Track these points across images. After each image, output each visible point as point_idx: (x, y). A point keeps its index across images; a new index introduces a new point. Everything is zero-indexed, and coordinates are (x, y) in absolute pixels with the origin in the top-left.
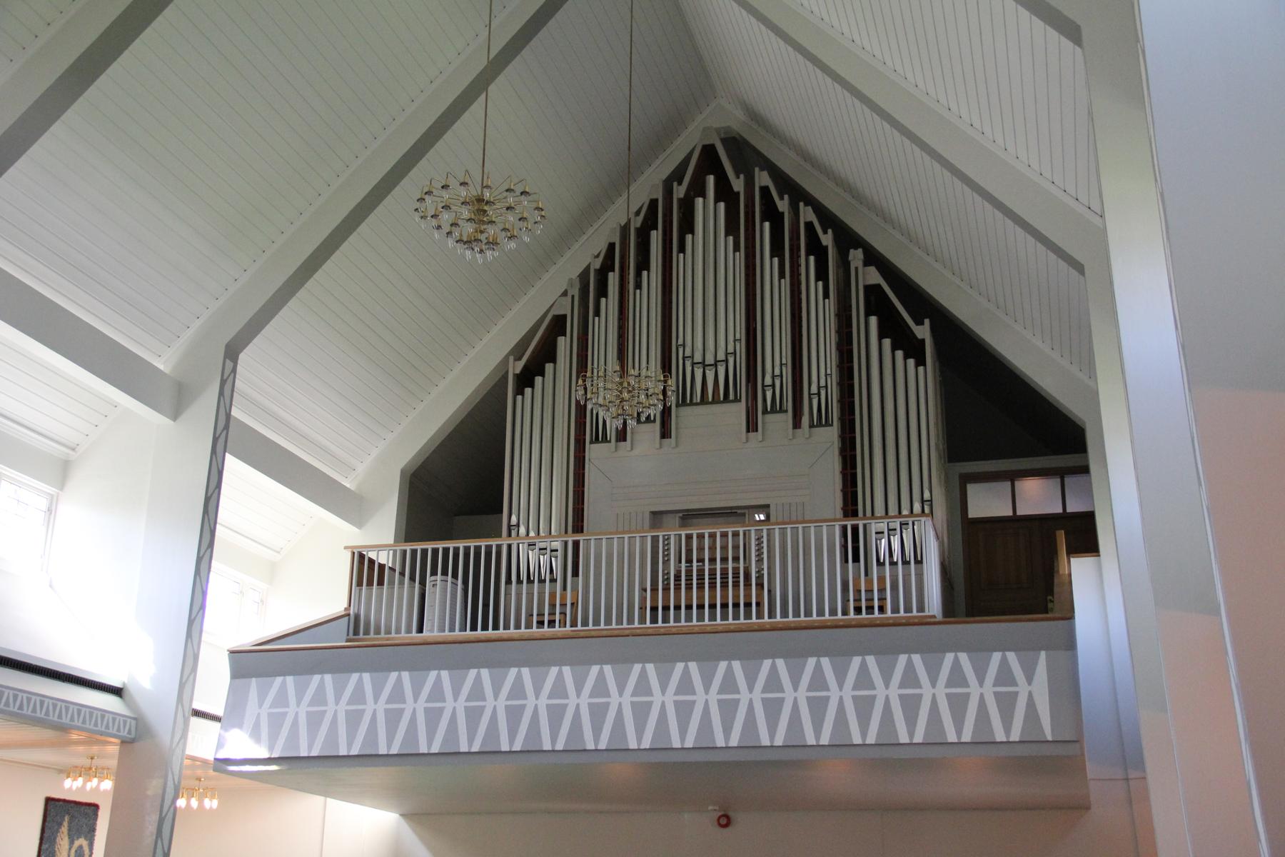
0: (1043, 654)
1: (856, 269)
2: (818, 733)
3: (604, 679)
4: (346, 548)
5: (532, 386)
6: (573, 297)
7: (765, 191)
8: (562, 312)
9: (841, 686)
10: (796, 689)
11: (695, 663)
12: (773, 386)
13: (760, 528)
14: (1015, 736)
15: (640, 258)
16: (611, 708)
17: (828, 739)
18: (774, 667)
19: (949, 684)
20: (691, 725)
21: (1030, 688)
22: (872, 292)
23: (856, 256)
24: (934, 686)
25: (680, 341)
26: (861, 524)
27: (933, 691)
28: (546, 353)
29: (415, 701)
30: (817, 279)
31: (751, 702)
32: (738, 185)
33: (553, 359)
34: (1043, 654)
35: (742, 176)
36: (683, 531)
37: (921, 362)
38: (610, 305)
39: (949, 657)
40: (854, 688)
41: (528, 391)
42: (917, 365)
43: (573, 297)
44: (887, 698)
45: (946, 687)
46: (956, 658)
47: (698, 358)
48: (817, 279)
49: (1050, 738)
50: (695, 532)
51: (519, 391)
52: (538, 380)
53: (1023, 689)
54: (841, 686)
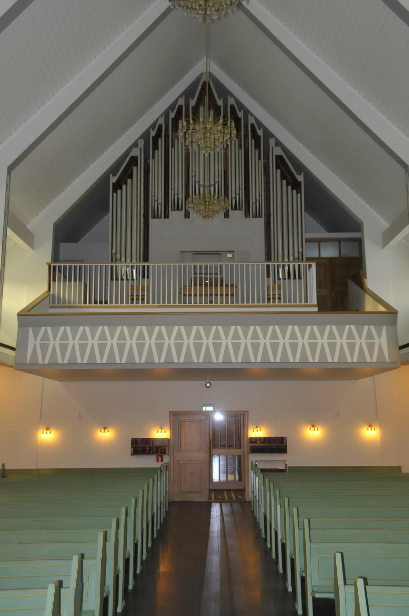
0: (30, 328)
1: (272, 148)
2: (159, 358)
3: (295, 332)
4: (47, 263)
5: (121, 189)
6: (141, 148)
7: (232, 107)
8: (135, 155)
9: (341, 338)
10: (284, 339)
11: (183, 327)
12: (236, 198)
13: (170, 264)
14: (375, 360)
15: (157, 133)
16: (241, 345)
17: (299, 360)
18: (103, 329)
19: (252, 339)
20: (181, 356)
21: (380, 341)
22: (279, 158)
23: (272, 142)
24: (246, 339)
25: (193, 174)
26: (114, 265)
27: (188, 341)
28: (127, 174)
29: (112, 340)
30: (255, 148)
31: (265, 344)
32: (220, 102)
33: (131, 177)
34: (385, 327)
35: (222, 99)
36: (193, 263)
37: (299, 191)
38: (160, 153)
39: (290, 327)
40: (232, 339)
41: (119, 191)
42: (297, 193)
43: (141, 148)
44: (322, 344)
45: (327, 339)
46: (122, 329)
47: (202, 183)
48: (255, 148)
49: (388, 361)
50: (198, 264)
51: (115, 190)
52: (124, 186)
53: (377, 340)
54: (341, 338)
